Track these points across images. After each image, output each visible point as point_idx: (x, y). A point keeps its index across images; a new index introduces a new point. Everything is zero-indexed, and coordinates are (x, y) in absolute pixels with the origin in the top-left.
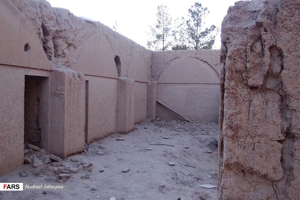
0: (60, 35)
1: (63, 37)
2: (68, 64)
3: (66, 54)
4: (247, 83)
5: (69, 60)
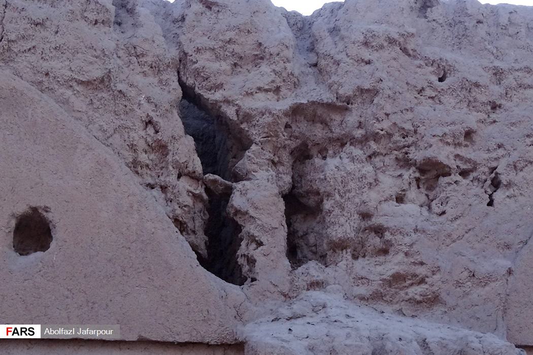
0: (337, 131)
1: (359, 133)
2: (415, 291)
3: (387, 229)
4: (295, 162)
5: (422, 264)
